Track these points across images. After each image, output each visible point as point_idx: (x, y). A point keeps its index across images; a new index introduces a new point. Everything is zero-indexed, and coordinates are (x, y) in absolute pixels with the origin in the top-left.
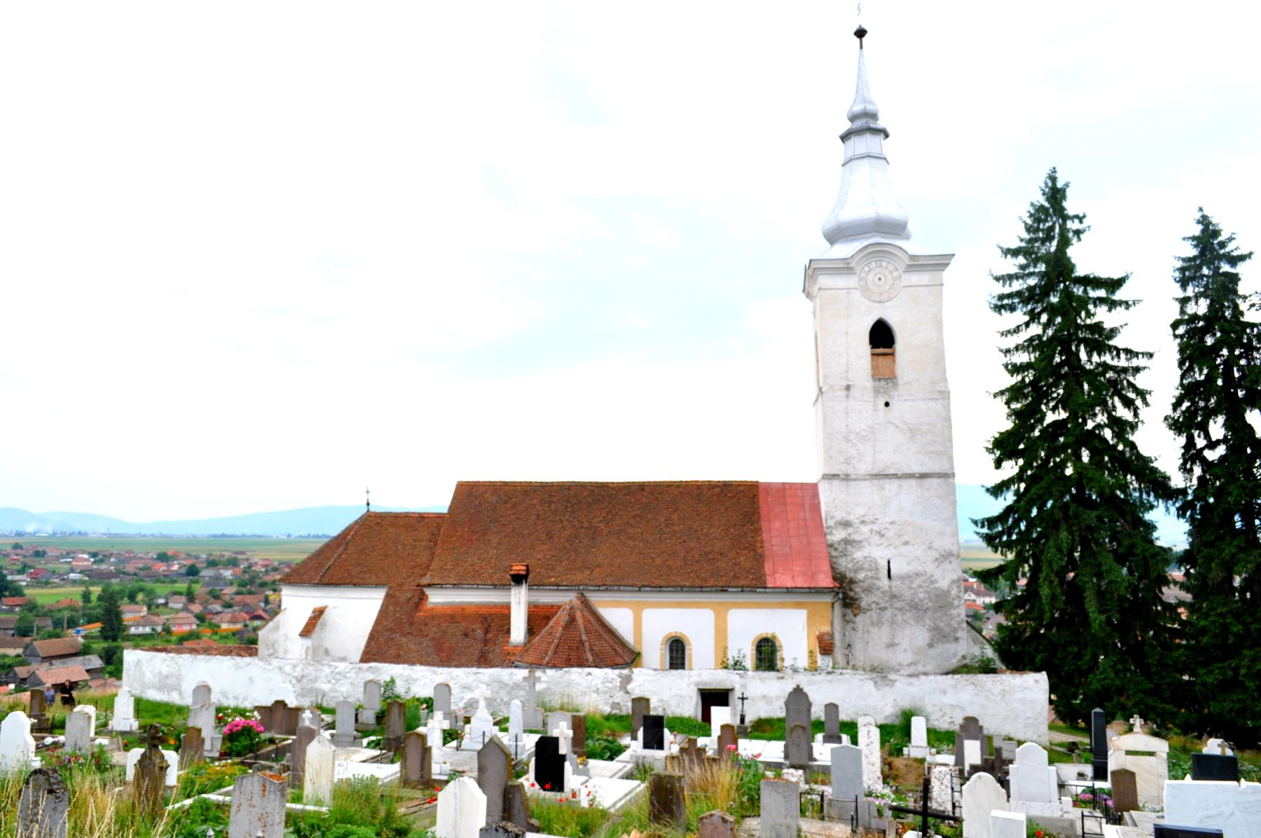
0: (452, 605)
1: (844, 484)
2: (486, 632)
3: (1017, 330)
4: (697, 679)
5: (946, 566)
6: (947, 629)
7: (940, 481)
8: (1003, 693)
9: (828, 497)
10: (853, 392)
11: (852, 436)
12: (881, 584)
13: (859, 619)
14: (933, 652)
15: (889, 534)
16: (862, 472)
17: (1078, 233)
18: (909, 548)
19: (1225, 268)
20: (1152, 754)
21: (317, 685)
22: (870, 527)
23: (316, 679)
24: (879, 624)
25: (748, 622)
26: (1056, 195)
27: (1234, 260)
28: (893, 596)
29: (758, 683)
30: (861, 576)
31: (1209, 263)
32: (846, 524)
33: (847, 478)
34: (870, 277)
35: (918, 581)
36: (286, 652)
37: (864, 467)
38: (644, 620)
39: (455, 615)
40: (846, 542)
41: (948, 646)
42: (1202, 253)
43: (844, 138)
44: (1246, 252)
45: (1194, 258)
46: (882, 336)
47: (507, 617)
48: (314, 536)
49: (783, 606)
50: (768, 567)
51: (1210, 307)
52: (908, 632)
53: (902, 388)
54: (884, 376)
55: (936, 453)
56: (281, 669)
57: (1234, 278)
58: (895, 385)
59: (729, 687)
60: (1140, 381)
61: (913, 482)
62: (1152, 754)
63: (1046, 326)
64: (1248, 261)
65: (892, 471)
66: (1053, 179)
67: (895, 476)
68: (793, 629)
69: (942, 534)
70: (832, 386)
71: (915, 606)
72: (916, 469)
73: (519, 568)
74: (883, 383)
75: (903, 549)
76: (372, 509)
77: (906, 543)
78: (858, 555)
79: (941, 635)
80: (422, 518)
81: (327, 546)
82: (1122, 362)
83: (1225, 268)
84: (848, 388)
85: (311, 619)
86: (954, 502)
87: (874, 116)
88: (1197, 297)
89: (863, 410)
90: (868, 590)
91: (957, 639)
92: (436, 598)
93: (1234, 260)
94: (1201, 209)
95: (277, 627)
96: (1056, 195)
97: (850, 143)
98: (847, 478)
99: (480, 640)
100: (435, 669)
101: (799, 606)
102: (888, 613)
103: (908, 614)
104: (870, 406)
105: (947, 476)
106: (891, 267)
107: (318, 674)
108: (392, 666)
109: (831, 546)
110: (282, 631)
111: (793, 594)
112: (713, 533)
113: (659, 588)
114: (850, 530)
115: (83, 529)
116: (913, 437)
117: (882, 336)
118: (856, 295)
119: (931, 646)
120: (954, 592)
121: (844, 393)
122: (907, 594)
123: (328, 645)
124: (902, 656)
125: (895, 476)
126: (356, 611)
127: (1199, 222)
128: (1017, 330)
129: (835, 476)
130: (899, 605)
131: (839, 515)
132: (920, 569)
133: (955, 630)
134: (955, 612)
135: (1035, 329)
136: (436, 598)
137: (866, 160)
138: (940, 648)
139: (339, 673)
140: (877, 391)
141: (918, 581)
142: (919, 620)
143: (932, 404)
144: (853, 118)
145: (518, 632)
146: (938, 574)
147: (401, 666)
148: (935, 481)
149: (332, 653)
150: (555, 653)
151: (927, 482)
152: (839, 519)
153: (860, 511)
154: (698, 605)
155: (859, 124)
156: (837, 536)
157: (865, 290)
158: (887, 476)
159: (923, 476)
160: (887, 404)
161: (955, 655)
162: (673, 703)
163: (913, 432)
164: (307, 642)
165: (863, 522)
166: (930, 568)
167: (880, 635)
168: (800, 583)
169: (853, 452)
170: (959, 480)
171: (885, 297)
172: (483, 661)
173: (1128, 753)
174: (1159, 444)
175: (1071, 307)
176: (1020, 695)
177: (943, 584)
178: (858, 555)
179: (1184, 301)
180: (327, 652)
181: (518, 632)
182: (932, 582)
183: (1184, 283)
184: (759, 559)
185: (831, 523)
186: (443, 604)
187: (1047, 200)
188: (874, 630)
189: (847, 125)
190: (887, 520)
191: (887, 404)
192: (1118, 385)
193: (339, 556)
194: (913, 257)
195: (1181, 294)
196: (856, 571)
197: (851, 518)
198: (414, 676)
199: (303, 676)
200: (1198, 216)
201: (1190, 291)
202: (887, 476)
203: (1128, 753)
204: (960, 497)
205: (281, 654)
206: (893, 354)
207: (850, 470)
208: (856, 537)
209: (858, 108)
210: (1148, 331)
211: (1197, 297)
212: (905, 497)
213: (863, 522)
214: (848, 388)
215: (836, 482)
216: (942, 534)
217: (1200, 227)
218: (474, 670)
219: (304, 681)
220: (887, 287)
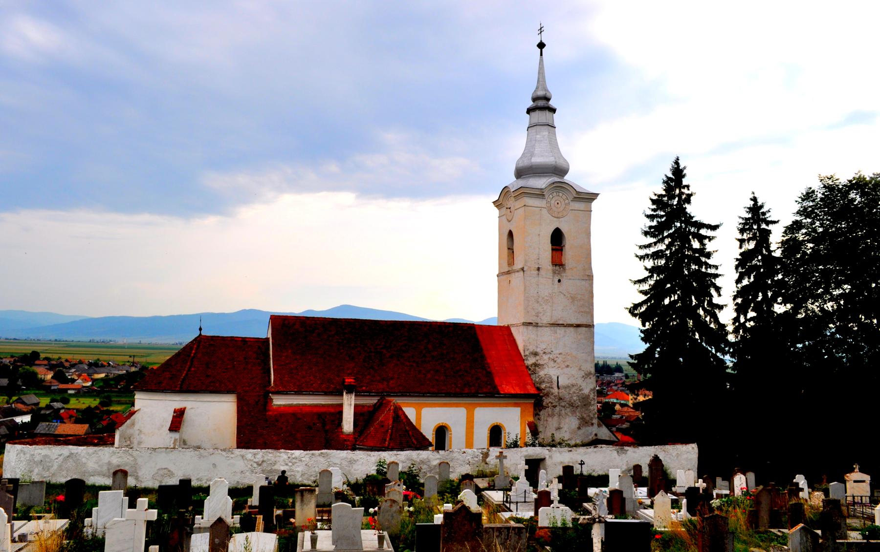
3: (649, 246)
4: (526, 453)
5: (588, 380)
6: (588, 418)
7: (587, 329)
8: (678, 455)
9: (521, 337)
11: (540, 300)
14: (580, 432)
15: (558, 361)
16: (545, 322)
17: (689, 196)
18: (569, 369)
19: (764, 226)
20: (863, 481)
21: (276, 467)
23: (275, 463)
24: (552, 415)
25: (487, 415)
26: (678, 173)
27: (768, 223)
28: (560, 399)
29: (558, 454)
30: (543, 386)
32: (536, 354)
33: (536, 325)
34: (553, 202)
35: (573, 390)
36: (140, 443)
37: (545, 319)
38: (427, 416)
39: (295, 413)
40: (536, 365)
41: (588, 428)
43: (529, 111)
45: (749, 219)
46: (557, 238)
47: (340, 413)
48: (128, 348)
49: (507, 405)
50: (497, 381)
51: (756, 245)
52: (567, 420)
53: (568, 272)
54: (558, 262)
55: (585, 312)
56: (243, 456)
58: (564, 269)
59: (542, 457)
60: (718, 282)
61: (572, 329)
62: (863, 481)
63: (669, 247)
64: (776, 225)
66: (677, 162)
67: (563, 325)
68: (512, 419)
69: (586, 361)
70: (530, 267)
71: (571, 405)
74: (557, 268)
75: (566, 370)
77: (568, 366)
78: (542, 373)
79: (585, 422)
81: (178, 355)
83: (764, 226)
84: (538, 269)
86: (593, 342)
88: (749, 240)
89: (546, 283)
90: (547, 395)
91: (592, 424)
92: (279, 401)
93: (768, 223)
95: (133, 424)
96: (678, 173)
97: (533, 114)
98: (536, 325)
99: (320, 432)
100: (370, 453)
101: (516, 405)
102: (558, 409)
103: (568, 410)
104: (550, 281)
105: (590, 326)
106: (564, 197)
107: (277, 459)
108: (339, 452)
109: (527, 367)
110: (137, 427)
111: (513, 398)
112: (457, 358)
114: (538, 358)
115: (614, 356)
116: (573, 301)
117: (557, 238)
118: (545, 211)
119: (579, 428)
122: (567, 397)
123: (185, 437)
124: (564, 434)
125: (563, 325)
128: (649, 246)
129: (530, 324)
130: (563, 404)
131: (532, 348)
132: (574, 382)
134: (592, 408)
135: (662, 247)
136: (279, 401)
140: (554, 272)
141: (573, 390)
142: (573, 412)
143: (583, 282)
145: (348, 425)
146: (584, 385)
147: (345, 452)
149: (188, 443)
150: (391, 439)
151: (580, 329)
152: (531, 350)
155: (541, 103)
156: (530, 361)
157: (550, 209)
159: (578, 326)
160: (559, 281)
161: (591, 434)
162: (512, 469)
163: (573, 299)
164: (176, 435)
165: (544, 353)
166: (580, 382)
167: (553, 423)
168: (518, 391)
169: (540, 309)
170: (596, 329)
171: (560, 215)
173: (855, 482)
174: (727, 316)
175: (682, 237)
176: (685, 456)
177: (586, 391)
179: (742, 241)
180: (185, 442)
181: (348, 425)
182: (581, 390)
183: (742, 231)
184: (489, 375)
185: (527, 353)
186: (285, 406)
187: (673, 174)
188: (550, 419)
189: (530, 104)
190: (558, 352)
191: (559, 281)
192: (705, 283)
194: (578, 193)
195: (740, 237)
197: (538, 350)
198: (355, 458)
199: (263, 461)
200: (752, 196)
201: (745, 236)
203: (855, 482)
204: (597, 338)
205: (135, 445)
207: (538, 321)
208: (541, 362)
209: (541, 93)
210: (724, 253)
211: (749, 240)
213: (544, 353)
214: (538, 269)
215: (530, 328)
216: (586, 361)
217: (752, 203)
218: (395, 452)
219: (265, 464)
220: (562, 209)
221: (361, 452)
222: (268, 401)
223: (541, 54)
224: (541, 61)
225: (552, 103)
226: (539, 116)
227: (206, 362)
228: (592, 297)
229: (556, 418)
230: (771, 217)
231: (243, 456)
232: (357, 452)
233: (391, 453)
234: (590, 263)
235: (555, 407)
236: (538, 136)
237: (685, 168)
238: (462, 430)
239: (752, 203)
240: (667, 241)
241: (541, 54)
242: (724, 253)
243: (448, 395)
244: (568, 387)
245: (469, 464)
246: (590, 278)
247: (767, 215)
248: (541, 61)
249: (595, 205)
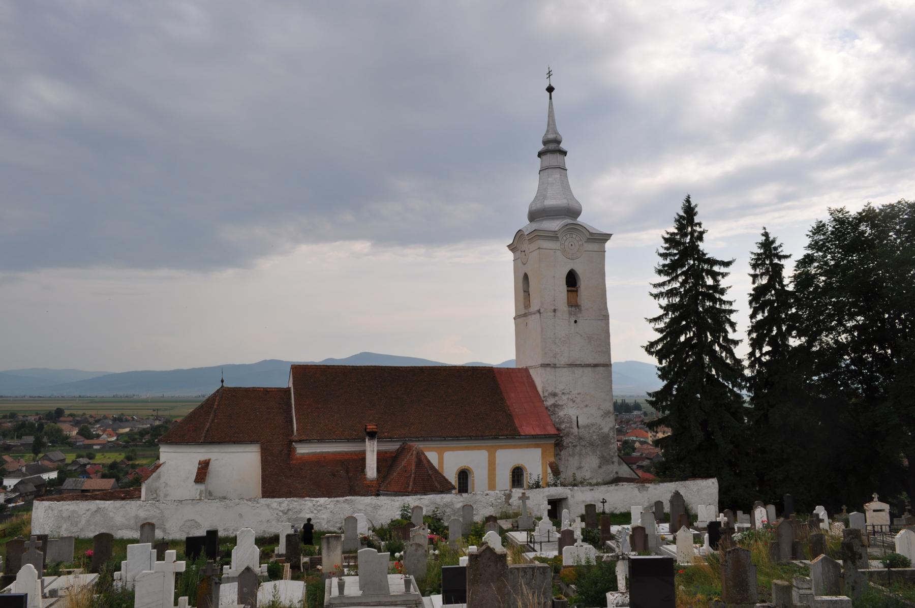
0: (314, 454)
1: (553, 370)
2: (348, 473)
3: (663, 284)
4: (548, 494)
8: (698, 491)
9: (540, 379)
10: (558, 313)
12: (573, 431)
13: (562, 453)
15: (577, 401)
21: (302, 515)
22: (567, 396)
24: (573, 455)
25: (509, 457)
27: (780, 257)
29: (580, 493)
30: (563, 426)
31: (767, 257)
32: (554, 395)
33: (555, 366)
34: (566, 243)
35: (593, 429)
36: (166, 496)
37: (563, 360)
38: (449, 460)
39: (320, 461)
40: (555, 405)
42: (765, 253)
43: (540, 155)
44: (788, 254)
46: (572, 280)
49: (528, 446)
54: (574, 305)
56: (268, 506)
57: (782, 266)
58: (580, 310)
61: (589, 369)
65: (578, 363)
66: (688, 201)
67: (580, 366)
68: (533, 461)
72: (592, 361)
73: (371, 427)
74: (573, 309)
76: (225, 385)
77: (587, 406)
78: (561, 414)
79: (605, 461)
80: (266, 392)
82: (727, 307)
83: (776, 261)
84: (555, 311)
85: (494, 469)
87: (558, 142)
88: (762, 274)
90: (568, 435)
91: (613, 463)
92: (302, 450)
93: (780, 257)
94: (765, 228)
95: (159, 477)
97: (544, 157)
98: (555, 366)
99: (344, 478)
101: (537, 446)
102: (578, 448)
106: (578, 238)
109: (547, 408)
110: (163, 480)
111: (534, 439)
113: (456, 438)
114: (557, 398)
118: (559, 253)
119: (600, 467)
120: (611, 435)
121: (552, 314)
125: (580, 366)
126: (240, 463)
127: (763, 235)
129: (548, 365)
130: (583, 443)
133: (612, 457)
134: (612, 446)
136: (302, 450)
137: (558, 170)
138: (604, 469)
139: (321, 506)
140: (570, 314)
141: (593, 429)
144: (545, 143)
145: (371, 471)
148: (601, 368)
150: (414, 484)
151: (598, 369)
153: (561, 387)
154: (478, 448)
155: (552, 146)
156: (550, 402)
157: (564, 251)
158: (576, 365)
159: (596, 366)
161: (612, 472)
164: (201, 487)
168: (538, 431)
172: (353, 492)
173: (874, 511)
175: (695, 275)
177: (606, 430)
178: (561, 414)
179: (755, 277)
180: (210, 494)
181: (371, 471)
183: (754, 266)
184: (510, 417)
185: (546, 394)
186: (308, 453)
188: (571, 459)
189: (541, 147)
191: (576, 322)
192: (719, 319)
193: (213, 421)
195: (752, 272)
196: (561, 423)
197: (557, 391)
199: (288, 510)
202: (576, 365)
203: (874, 511)
204: (614, 377)
205: (161, 498)
206: (577, 291)
207: (556, 362)
208: (560, 403)
209: (551, 136)
210: (738, 288)
211: (762, 274)
212: (586, 377)
214: (555, 311)
215: (549, 369)
217: (764, 238)
218: (419, 497)
219: (290, 513)
223: (551, 98)
224: (551, 104)
225: (563, 146)
226: (551, 159)
227: (228, 412)
229: (576, 458)
231: (268, 506)
234: (606, 303)
235: (575, 446)
238: (484, 472)
239: (764, 238)
241: (551, 98)
242: (738, 288)
243: (470, 438)
245: (492, 505)
246: (606, 317)
248: (551, 104)
249: (608, 245)
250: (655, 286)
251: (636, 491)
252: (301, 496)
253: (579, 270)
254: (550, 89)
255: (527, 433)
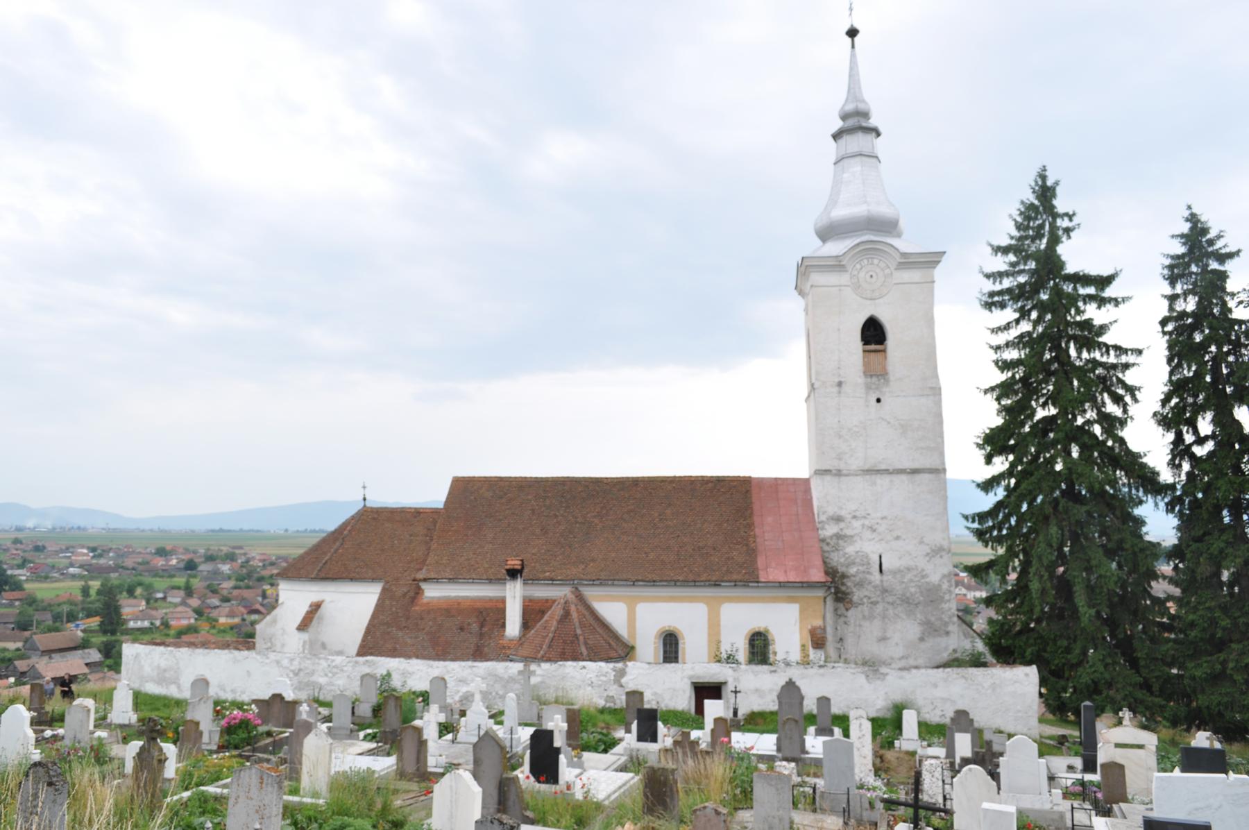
0: (447, 599)
1: (836, 479)
2: (482, 626)
3: (1007, 327)
4: (691, 673)
5: (937, 560)
6: (938, 623)
8: (994, 687)
9: (819, 492)
10: (845, 388)
12: (872, 578)
14: (923, 646)
15: (881, 529)
16: (854, 467)
18: (900, 543)
19: (1214, 265)
20: (1140, 747)
21: (314, 678)
23: (313, 673)
24: (871, 618)
25: (741, 616)
26: (1046, 193)
28: (885, 591)
30: (853, 570)
32: (838, 519)
33: (839, 473)
34: (862, 275)
35: (909, 576)
37: (855, 463)
38: (638, 614)
39: (451, 609)
40: (838, 536)
41: (939, 640)
42: (1191, 251)
43: (836, 136)
46: (873, 332)
50: (761, 562)
51: (1199, 304)
54: (876, 373)
56: (278, 662)
57: (1223, 276)
58: (887, 381)
59: (722, 680)
60: (1130, 377)
61: (904, 477)
62: (1140, 747)
64: (1236, 260)
65: (883, 467)
66: (1043, 177)
67: (887, 472)
68: (786, 623)
72: (908, 464)
73: (514, 563)
74: (874, 379)
76: (368, 505)
77: (898, 538)
78: (850, 550)
79: (932, 629)
83: (1214, 265)
84: (840, 384)
85: (308, 613)
87: (865, 115)
88: (1186, 294)
90: (860, 585)
91: (947, 633)
92: (432, 592)
93: (1223, 258)
94: (1189, 207)
95: (275, 621)
98: (839, 473)
99: (475, 634)
100: (431, 662)
101: (791, 600)
102: (880, 608)
103: (900, 609)
106: (882, 265)
109: (823, 540)
112: (704, 528)
113: (653, 583)
114: (842, 525)
117: (873, 332)
119: (922, 639)
121: (836, 389)
124: (894, 649)
125: (887, 472)
126: (353, 605)
127: (1187, 220)
128: (1007, 327)
129: (827, 472)
130: (890, 599)
131: (832, 510)
132: (911, 563)
133: (946, 624)
134: (945, 606)
136: (432, 592)
137: (858, 159)
138: (930, 642)
139: (336, 667)
140: (868, 388)
141: (909, 576)
144: (844, 117)
145: (513, 626)
146: (929, 568)
147: (397, 660)
148: (927, 476)
150: (550, 646)
151: (918, 477)
155: (851, 122)
156: (829, 531)
157: (857, 287)
158: (878, 472)
159: (915, 471)
161: (946, 649)
164: (305, 636)
165: (854, 517)
166: (922, 563)
167: (872, 629)
168: (792, 577)
172: (479, 654)
173: (1118, 745)
174: (1148, 440)
175: (1062, 304)
177: (934, 578)
178: (850, 550)
179: (1172, 299)
180: (324, 646)
181: (513, 626)
182: (923, 577)
183: (1172, 280)
184: (752, 553)
185: (823, 518)
186: (439, 598)
187: (1037, 198)
188: (866, 624)
189: (838, 124)
190: (879, 515)
191: (878, 400)
192: (1109, 381)
194: (904, 255)
196: (848, 566)
197: (843, 513)
198: (410, 669)
199: (300, 670)
200: (1187, 214)
201: (1179, 289)
202: (878, 472)
203: (1118, 745)
204: (950, 493)
205: (278, 648)
206: (884, 351)
207: (842, 466)
208: (848, 532)
210: (1137, 324)
211: (1186, 294)
212: (896, 493)
213: (854, 517)
214: (840, 384)
215: (828, 478)
217: (1188, 225)
218: (470, 663)
219: (302, 674)
221: (419, 661)
222: (419, 591)
223: (853, 46)
224: (853, 56)
225: (873, 122)
226: (857, 142)
227: (366, 544)
228: (941, 423)
229: (877, 623)
230: (1226, 244)
231: (278, 662)
232: (414, 661)
233: (463, 663)
234: (936, 368)
235: (875, 603)
236: (845, 175)
237: (1057, 183)
238: (672, 637)
239: (1188, 225)
240: (1034, 315)
241: (853, 46)
242: (1137, 324)
243: (675, 583)
244: (900, 571)
245: (591, 684)
246: (936, 391)
247: (1219, 244)
248: (853, 56)
249: (939, 272)
250: (996, 330)
251: (862, 679)
252: (408, 657)
253: (885, 318)
254: (852, 33)
255: (771, 578)
